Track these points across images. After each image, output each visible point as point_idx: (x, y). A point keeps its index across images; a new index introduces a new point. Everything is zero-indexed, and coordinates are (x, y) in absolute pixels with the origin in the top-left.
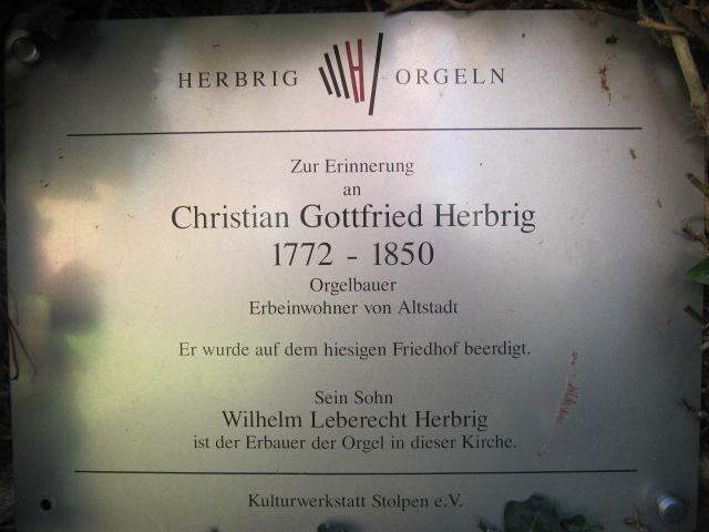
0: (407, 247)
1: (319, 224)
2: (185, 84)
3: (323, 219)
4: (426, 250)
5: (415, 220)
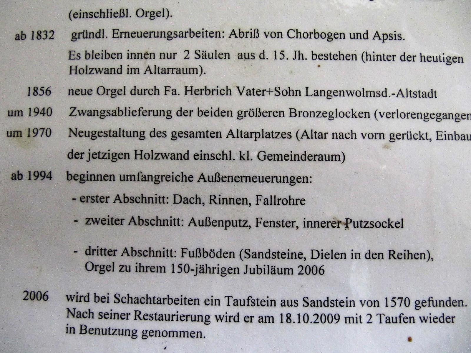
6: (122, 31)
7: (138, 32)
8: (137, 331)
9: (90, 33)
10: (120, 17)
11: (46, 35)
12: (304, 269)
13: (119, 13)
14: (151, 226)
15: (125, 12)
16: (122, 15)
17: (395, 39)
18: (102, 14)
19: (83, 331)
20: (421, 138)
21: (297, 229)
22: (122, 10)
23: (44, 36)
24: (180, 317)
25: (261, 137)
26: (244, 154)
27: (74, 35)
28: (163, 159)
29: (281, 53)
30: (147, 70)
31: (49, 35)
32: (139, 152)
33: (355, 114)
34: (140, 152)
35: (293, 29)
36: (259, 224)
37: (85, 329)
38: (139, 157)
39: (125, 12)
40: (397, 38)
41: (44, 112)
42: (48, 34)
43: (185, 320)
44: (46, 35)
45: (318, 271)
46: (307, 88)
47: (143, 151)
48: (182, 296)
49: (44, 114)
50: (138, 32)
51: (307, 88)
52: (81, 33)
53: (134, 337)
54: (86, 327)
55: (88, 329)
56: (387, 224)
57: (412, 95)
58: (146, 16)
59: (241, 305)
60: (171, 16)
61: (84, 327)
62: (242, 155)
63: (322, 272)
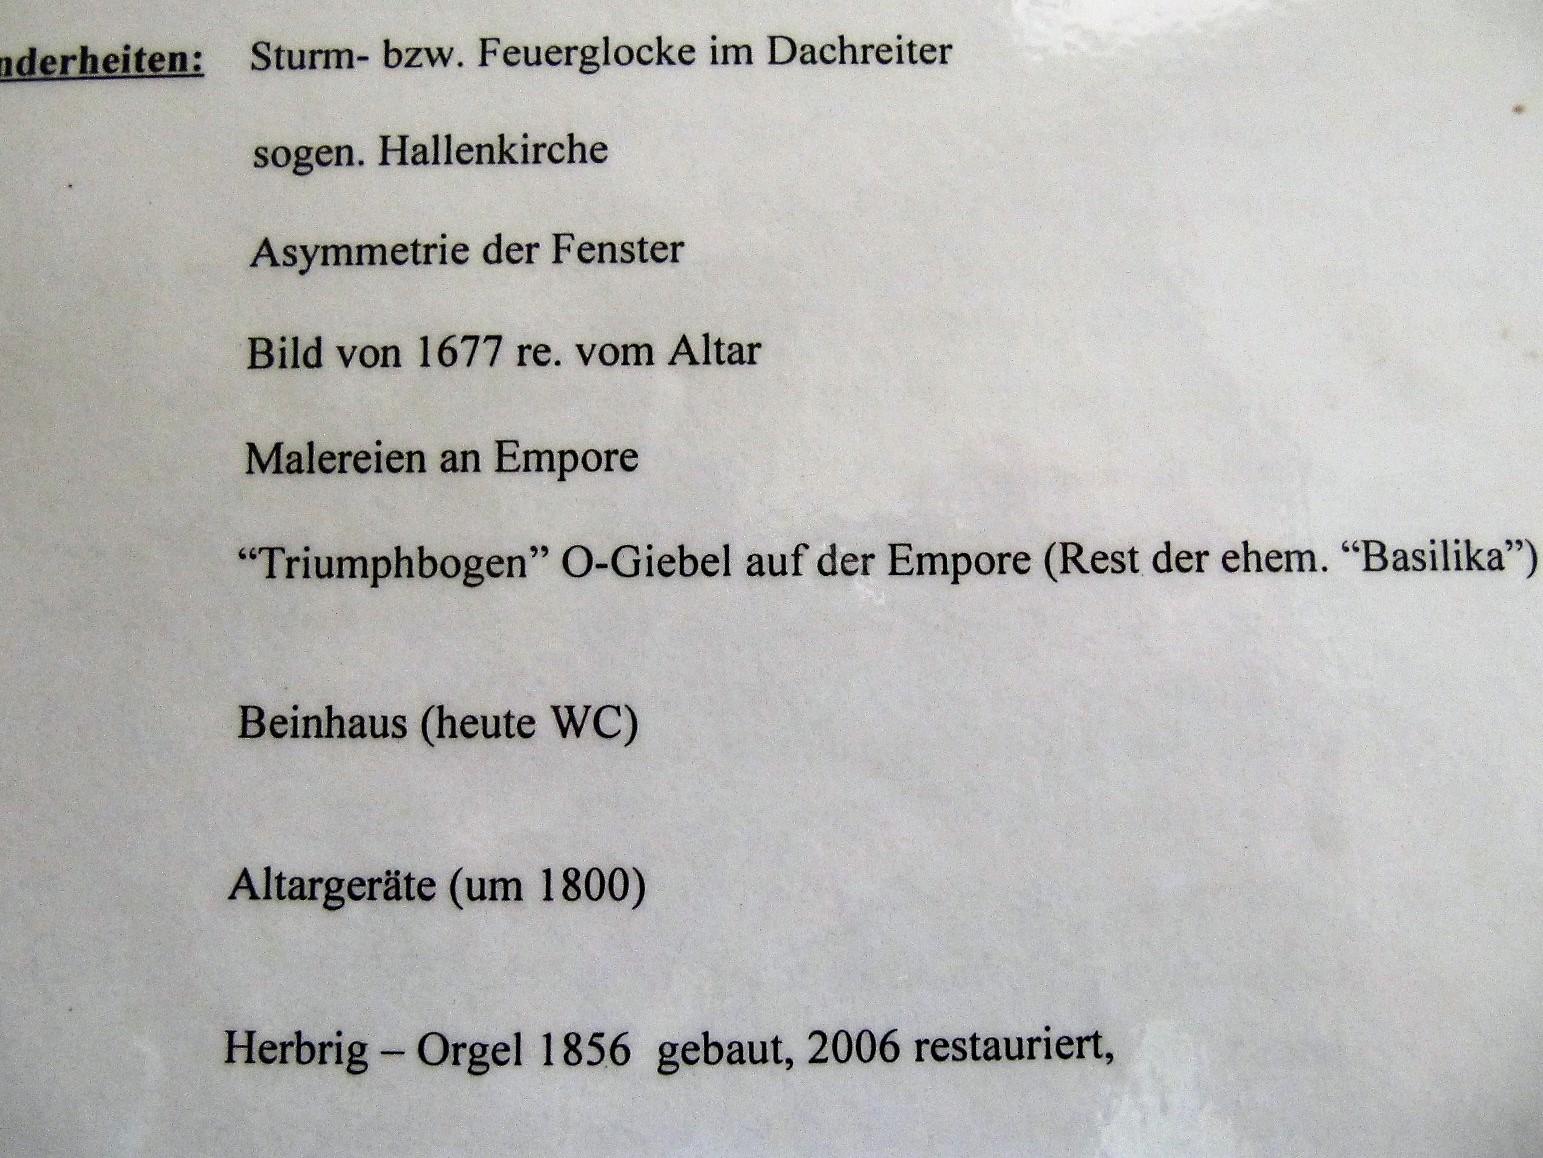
8: (367, 1048)
12: (830, 1041)
19: (253, 729)
20: (663, 58)
21: (788, 1069)
26: (512, 145)
28: (433, 65)
29: (592, 1043)
30: (241, 885)
32: (240, 1039)
34: (399, 141)
36: (563, 254)
37: (258, 721)
38: (240, 1055)
43: (506, 574)
45: (877, 1048)
47: (255, 1036)
53: (355, 1067)
54: (261, 713)
55: (266, 721)
56: (655, 54)
61: (252, 715)
63: (890, 1052)
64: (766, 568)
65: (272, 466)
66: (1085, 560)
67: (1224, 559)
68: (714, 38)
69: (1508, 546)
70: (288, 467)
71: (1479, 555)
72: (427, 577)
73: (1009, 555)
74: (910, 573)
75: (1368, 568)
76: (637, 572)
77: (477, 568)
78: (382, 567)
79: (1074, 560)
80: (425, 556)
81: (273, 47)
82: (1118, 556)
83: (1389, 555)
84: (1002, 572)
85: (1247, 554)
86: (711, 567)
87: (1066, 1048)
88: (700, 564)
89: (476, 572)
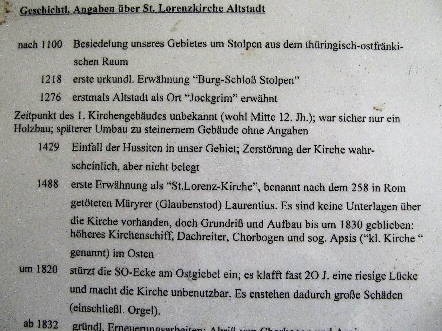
0: (360, 185)
1: (204, 132)
2: (127, 145)
3: (175, 44)
4: (360, 223)
5: (261, 225)
6: (117, 326)
7: (130, 327)
9: (89, 326)
10: (114, 312)
11: (50, 324)
13: (113, 308)
14: (76, 132)
15: (119, 308)
16: (116, 310)
17: (350, 241)
18: (99, 309)
22: (116, 306)
23: (49, 326)
24: (229, 149)
25: (207, 204)
27: (75, 326)
31: (54, 324)
33: (321, 206)
35: (206, 219)
39: (119, 308)
40: (352, 239)
41: (45, 183)
42: (52, 323)
44: (50, 324)
46: (227, 202)
48: (187, 326)
49: (45, 185)
50: (130, 327)
51: (227, 202)
52: (81, 325)
57: (127, 99)
58: (137, 313)
59: (272, 47)
60: (159, 314)
62: (259, 274)
64: (222, 132)
65: (122, 205)
66: (108, 62)
67: (388, 119)
68: (167, 144)
69: (227, 241)
70: (87, 255)
71: (322, 206)
72: (184, 208)
73: (200, 185)
74: (101, 188)
75: (199, 82)
76: (166, 207)
77: (219, 81)
78: (64, 130)
79: (387, 188)
80: (130, 164)
81: (234, 41)
82: (370, 275)
83: (205, 79)
84: (176, 101)
85: (275, 293)
86: (215, 276)
87: (253, 10)
88: (355, 296)
89: (219, 82)
